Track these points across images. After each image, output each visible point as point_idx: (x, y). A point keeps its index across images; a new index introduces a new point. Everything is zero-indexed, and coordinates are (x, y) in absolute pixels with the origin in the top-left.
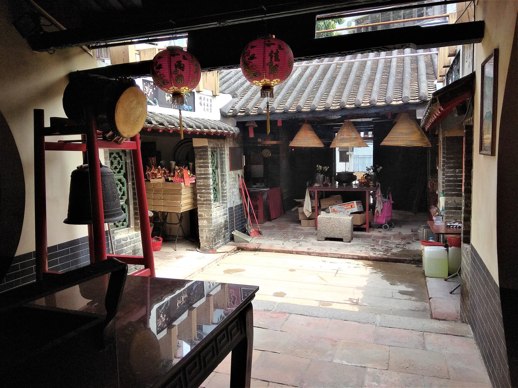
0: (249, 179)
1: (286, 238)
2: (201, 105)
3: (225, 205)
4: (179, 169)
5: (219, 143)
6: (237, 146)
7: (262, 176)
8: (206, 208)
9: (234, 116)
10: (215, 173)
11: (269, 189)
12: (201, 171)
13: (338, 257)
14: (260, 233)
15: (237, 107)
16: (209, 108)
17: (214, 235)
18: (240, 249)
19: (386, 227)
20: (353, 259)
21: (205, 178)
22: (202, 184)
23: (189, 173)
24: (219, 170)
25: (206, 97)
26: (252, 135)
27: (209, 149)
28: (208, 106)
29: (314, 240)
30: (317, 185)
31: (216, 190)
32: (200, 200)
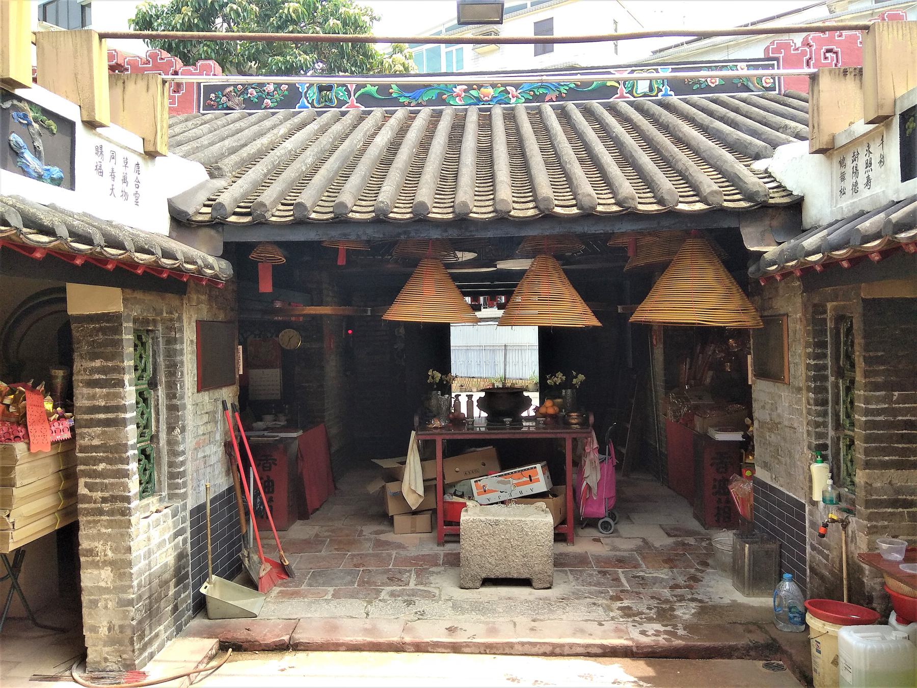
0: (249, 408)
1: (366, 587)
2: (101, 173)
3: (178, 504)
4: (12, 392)
5: (162, 304)
6: (221, 317)
7: (279, 397)
8: (110, 524)
9: (217, 223)
10: (145, 400)
11: (300, 433)
12: (94, 397)
13: (545, 654)
14: (284, 571)
15: (225, 199)
16: (131, 189)
17: (138, 617)
18: (232, 646)
19: (606, 526)
20: (588, 655)
21: (108, 423)
22: (96, 442)
23: (49, 406)
24: (161, 392)
25: (121, 154)
26: (266, 286)
27: (128, 325)
28: (125, 180)
29: (445, 586)
30: (436, 423)
31: (148, 457)
32: (89, 500)
